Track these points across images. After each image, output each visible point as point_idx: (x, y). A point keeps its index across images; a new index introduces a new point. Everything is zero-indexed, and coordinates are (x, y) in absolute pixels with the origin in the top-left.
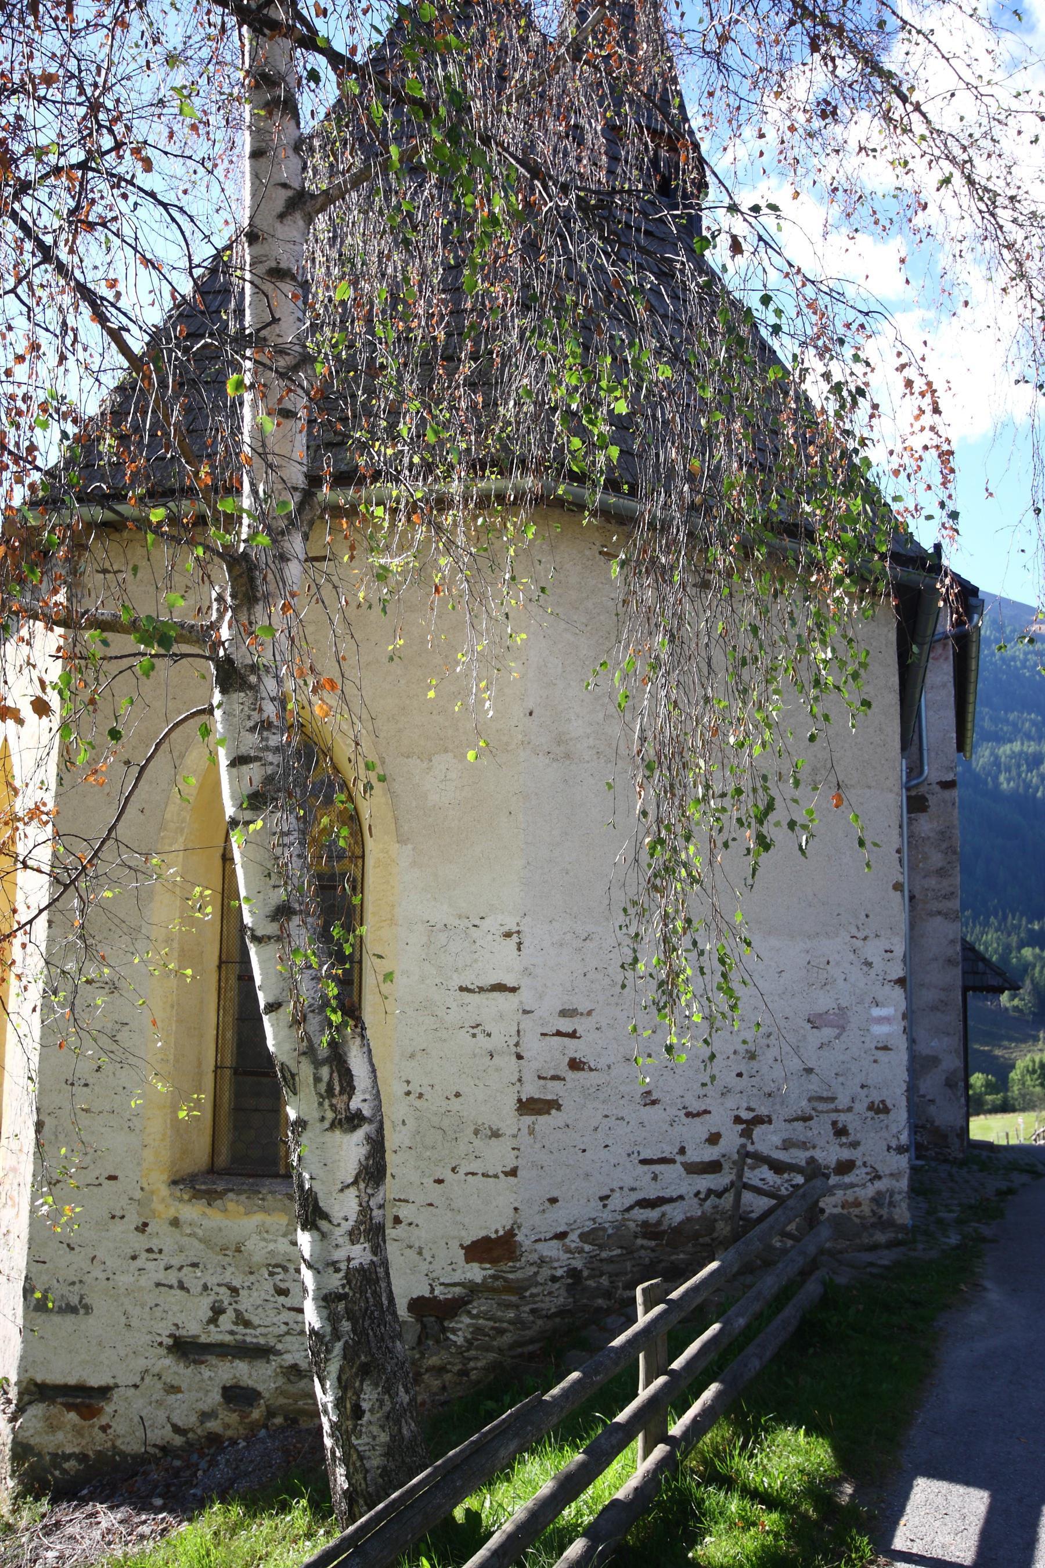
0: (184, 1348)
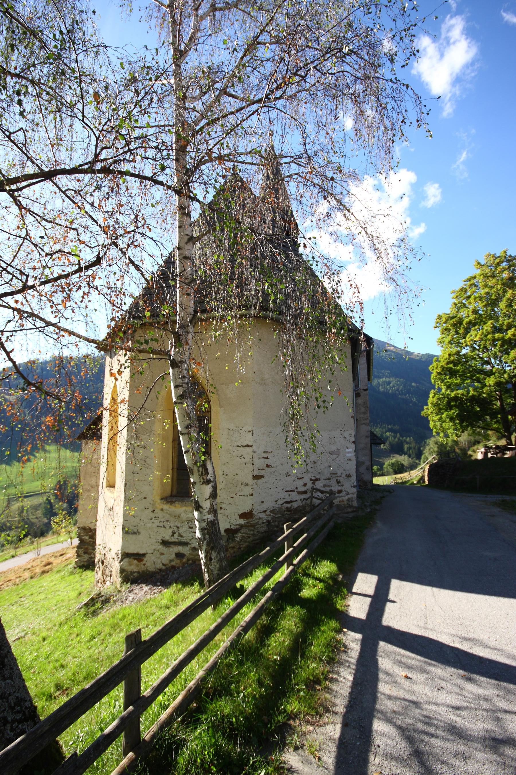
0: (165, 543)
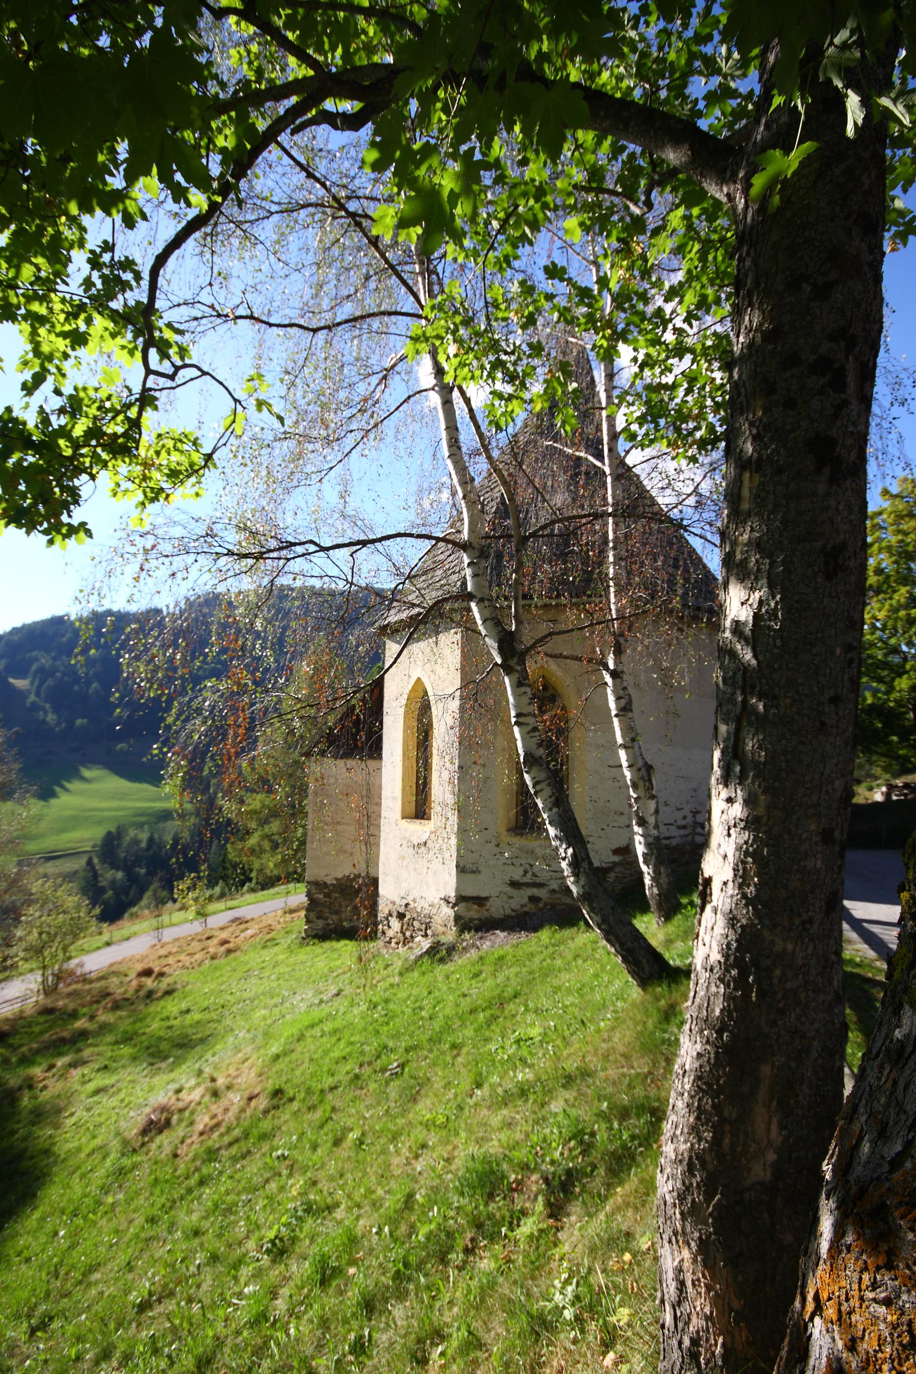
0: (514, 884)
